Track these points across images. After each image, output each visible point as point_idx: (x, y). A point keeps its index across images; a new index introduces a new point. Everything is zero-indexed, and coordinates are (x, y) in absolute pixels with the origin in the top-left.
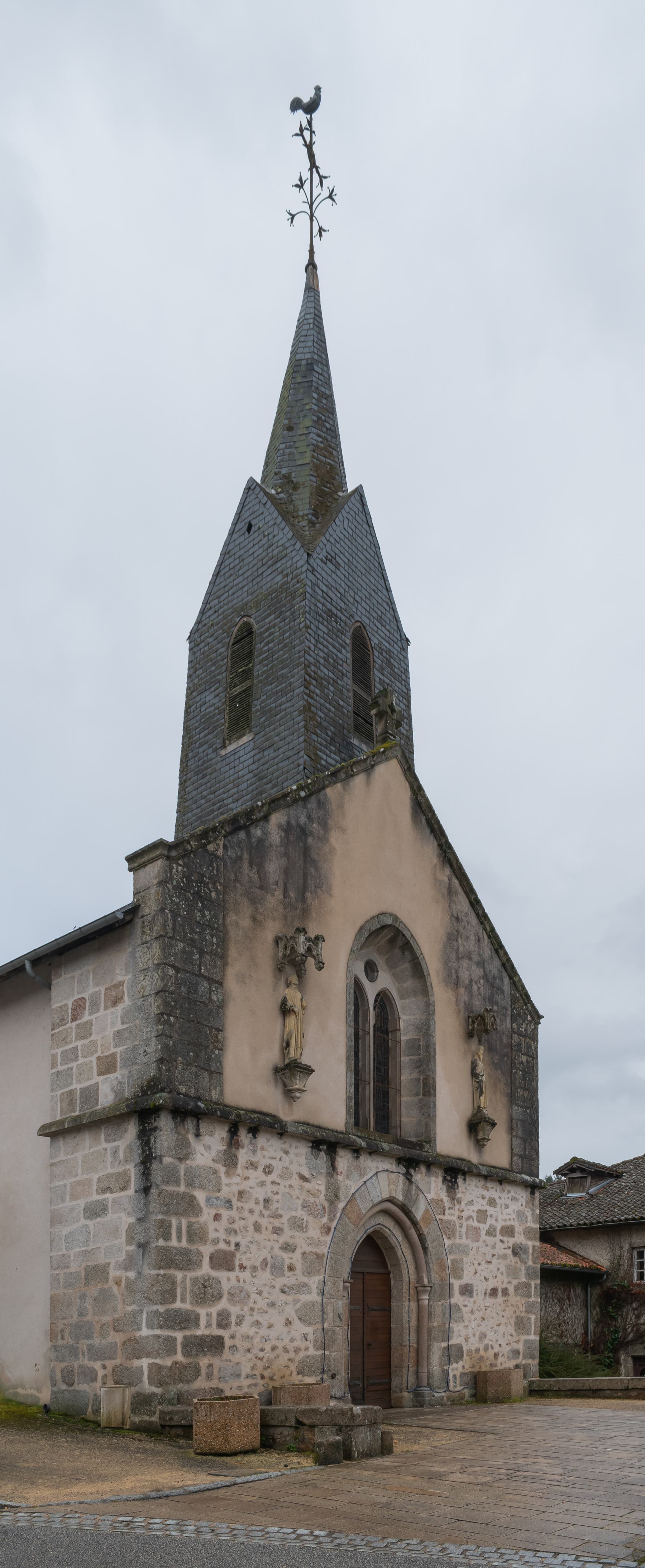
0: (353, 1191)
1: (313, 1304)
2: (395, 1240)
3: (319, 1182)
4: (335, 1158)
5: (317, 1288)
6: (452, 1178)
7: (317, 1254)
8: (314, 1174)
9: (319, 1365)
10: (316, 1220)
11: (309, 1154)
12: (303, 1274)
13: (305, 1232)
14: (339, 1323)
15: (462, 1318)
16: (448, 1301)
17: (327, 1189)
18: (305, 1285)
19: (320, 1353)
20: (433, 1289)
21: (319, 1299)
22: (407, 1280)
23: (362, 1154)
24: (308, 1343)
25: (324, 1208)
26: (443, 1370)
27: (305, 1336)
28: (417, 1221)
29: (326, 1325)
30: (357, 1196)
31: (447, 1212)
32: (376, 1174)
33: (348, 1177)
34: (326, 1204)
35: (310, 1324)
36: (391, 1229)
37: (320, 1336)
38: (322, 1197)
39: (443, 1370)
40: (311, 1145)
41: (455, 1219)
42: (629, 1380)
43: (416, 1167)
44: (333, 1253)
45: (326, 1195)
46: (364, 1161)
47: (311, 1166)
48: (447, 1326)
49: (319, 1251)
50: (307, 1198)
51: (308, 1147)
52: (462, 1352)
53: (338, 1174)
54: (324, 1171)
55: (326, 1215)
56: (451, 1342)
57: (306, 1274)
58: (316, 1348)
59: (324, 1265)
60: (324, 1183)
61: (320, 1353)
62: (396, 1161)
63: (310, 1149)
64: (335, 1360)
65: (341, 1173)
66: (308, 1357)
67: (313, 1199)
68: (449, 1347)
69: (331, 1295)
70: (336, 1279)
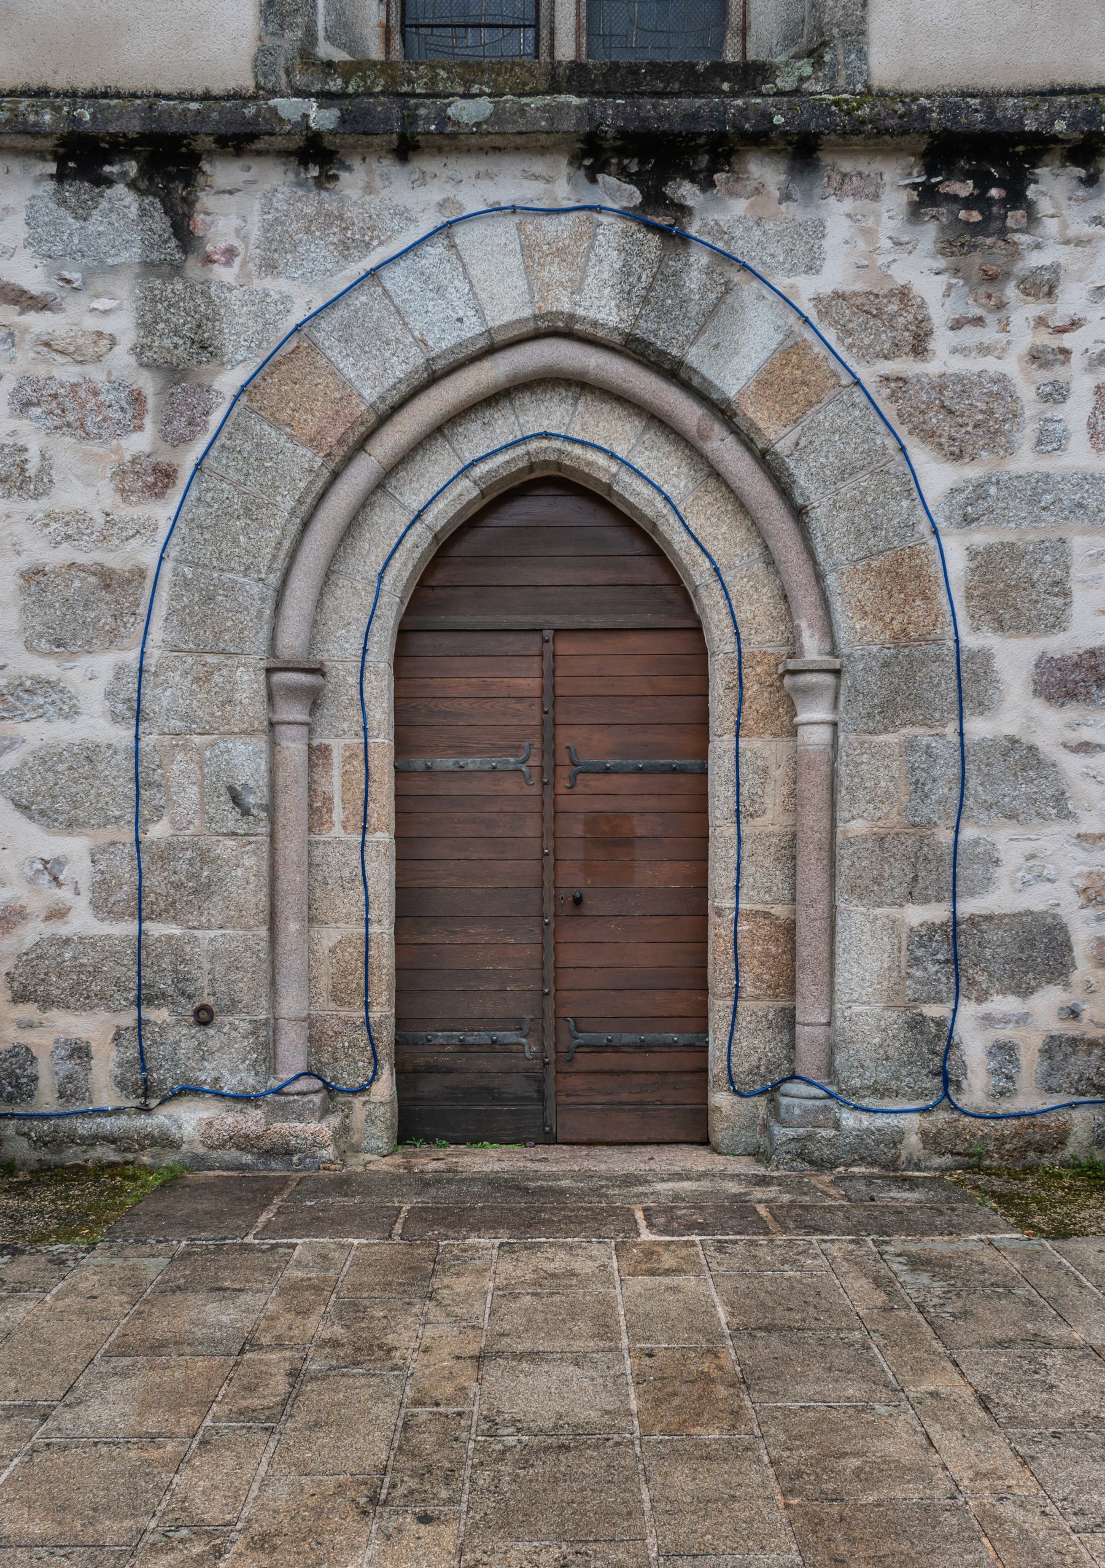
0: (298, 315)
1: (91, 754)
2: (646, 491)
3: (103, 304)
4: (189, 202)
5: (110, 694)
6: (983, 182)
7: (106, 578)
8: (75, 276)
9: (127, 971)
10: (94, 447)
11: (48, 208)
12: (29, 647)
13: (36, 497)
14: (231, 818)
15: (1060, 799)
16: (951, 729)
17: (147, 326)
18: (44, 684)
19: (127, 928)
20: (847, 681)
21: (123, 735)
22: (731, 648)
23: (356, 163)
24: (65, 894)
25: (137, 399)
26: (917, 1024)
27: (52, 869)
28: (728, 401)
29: (158, 831)
30: (324, 333)
31: (941, 341)
32: (445, 229)
33: (270, 267)
34: (148, 384)
35: (72, 825)
36: (621, 450)
37: (126, 871)
38: (122, 359)
39: (917, 1024)
40: (52, 168)
41: (1011, 366)
42: (925, 1178)
43: (713, 169)
44: (194, 564)
45: (139, 350)
46: (369, 189)
47: (58, 249)
48: (944, 836)
49: (115, 560)
50: (41, 371)
51: (39, 179)
52: (1066, 946)
53: (209, 260)
54: (132, 254)
55: (148, 422)
56: (968, 907)
57: (44, 645)
58: (102, 907)
59: (143, 610)
60: (129, 305)
61: (127, 928)
62: (575, 160)
63: (51, 185)
64: (214, 957)
65: (230, 253)
66: (67, 941)
67: (77, 369)
68: (954, 928)
69: (187, 717)
70: (211, 659)
